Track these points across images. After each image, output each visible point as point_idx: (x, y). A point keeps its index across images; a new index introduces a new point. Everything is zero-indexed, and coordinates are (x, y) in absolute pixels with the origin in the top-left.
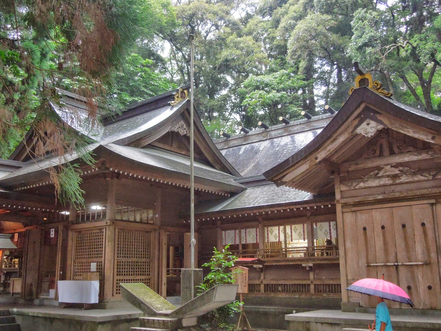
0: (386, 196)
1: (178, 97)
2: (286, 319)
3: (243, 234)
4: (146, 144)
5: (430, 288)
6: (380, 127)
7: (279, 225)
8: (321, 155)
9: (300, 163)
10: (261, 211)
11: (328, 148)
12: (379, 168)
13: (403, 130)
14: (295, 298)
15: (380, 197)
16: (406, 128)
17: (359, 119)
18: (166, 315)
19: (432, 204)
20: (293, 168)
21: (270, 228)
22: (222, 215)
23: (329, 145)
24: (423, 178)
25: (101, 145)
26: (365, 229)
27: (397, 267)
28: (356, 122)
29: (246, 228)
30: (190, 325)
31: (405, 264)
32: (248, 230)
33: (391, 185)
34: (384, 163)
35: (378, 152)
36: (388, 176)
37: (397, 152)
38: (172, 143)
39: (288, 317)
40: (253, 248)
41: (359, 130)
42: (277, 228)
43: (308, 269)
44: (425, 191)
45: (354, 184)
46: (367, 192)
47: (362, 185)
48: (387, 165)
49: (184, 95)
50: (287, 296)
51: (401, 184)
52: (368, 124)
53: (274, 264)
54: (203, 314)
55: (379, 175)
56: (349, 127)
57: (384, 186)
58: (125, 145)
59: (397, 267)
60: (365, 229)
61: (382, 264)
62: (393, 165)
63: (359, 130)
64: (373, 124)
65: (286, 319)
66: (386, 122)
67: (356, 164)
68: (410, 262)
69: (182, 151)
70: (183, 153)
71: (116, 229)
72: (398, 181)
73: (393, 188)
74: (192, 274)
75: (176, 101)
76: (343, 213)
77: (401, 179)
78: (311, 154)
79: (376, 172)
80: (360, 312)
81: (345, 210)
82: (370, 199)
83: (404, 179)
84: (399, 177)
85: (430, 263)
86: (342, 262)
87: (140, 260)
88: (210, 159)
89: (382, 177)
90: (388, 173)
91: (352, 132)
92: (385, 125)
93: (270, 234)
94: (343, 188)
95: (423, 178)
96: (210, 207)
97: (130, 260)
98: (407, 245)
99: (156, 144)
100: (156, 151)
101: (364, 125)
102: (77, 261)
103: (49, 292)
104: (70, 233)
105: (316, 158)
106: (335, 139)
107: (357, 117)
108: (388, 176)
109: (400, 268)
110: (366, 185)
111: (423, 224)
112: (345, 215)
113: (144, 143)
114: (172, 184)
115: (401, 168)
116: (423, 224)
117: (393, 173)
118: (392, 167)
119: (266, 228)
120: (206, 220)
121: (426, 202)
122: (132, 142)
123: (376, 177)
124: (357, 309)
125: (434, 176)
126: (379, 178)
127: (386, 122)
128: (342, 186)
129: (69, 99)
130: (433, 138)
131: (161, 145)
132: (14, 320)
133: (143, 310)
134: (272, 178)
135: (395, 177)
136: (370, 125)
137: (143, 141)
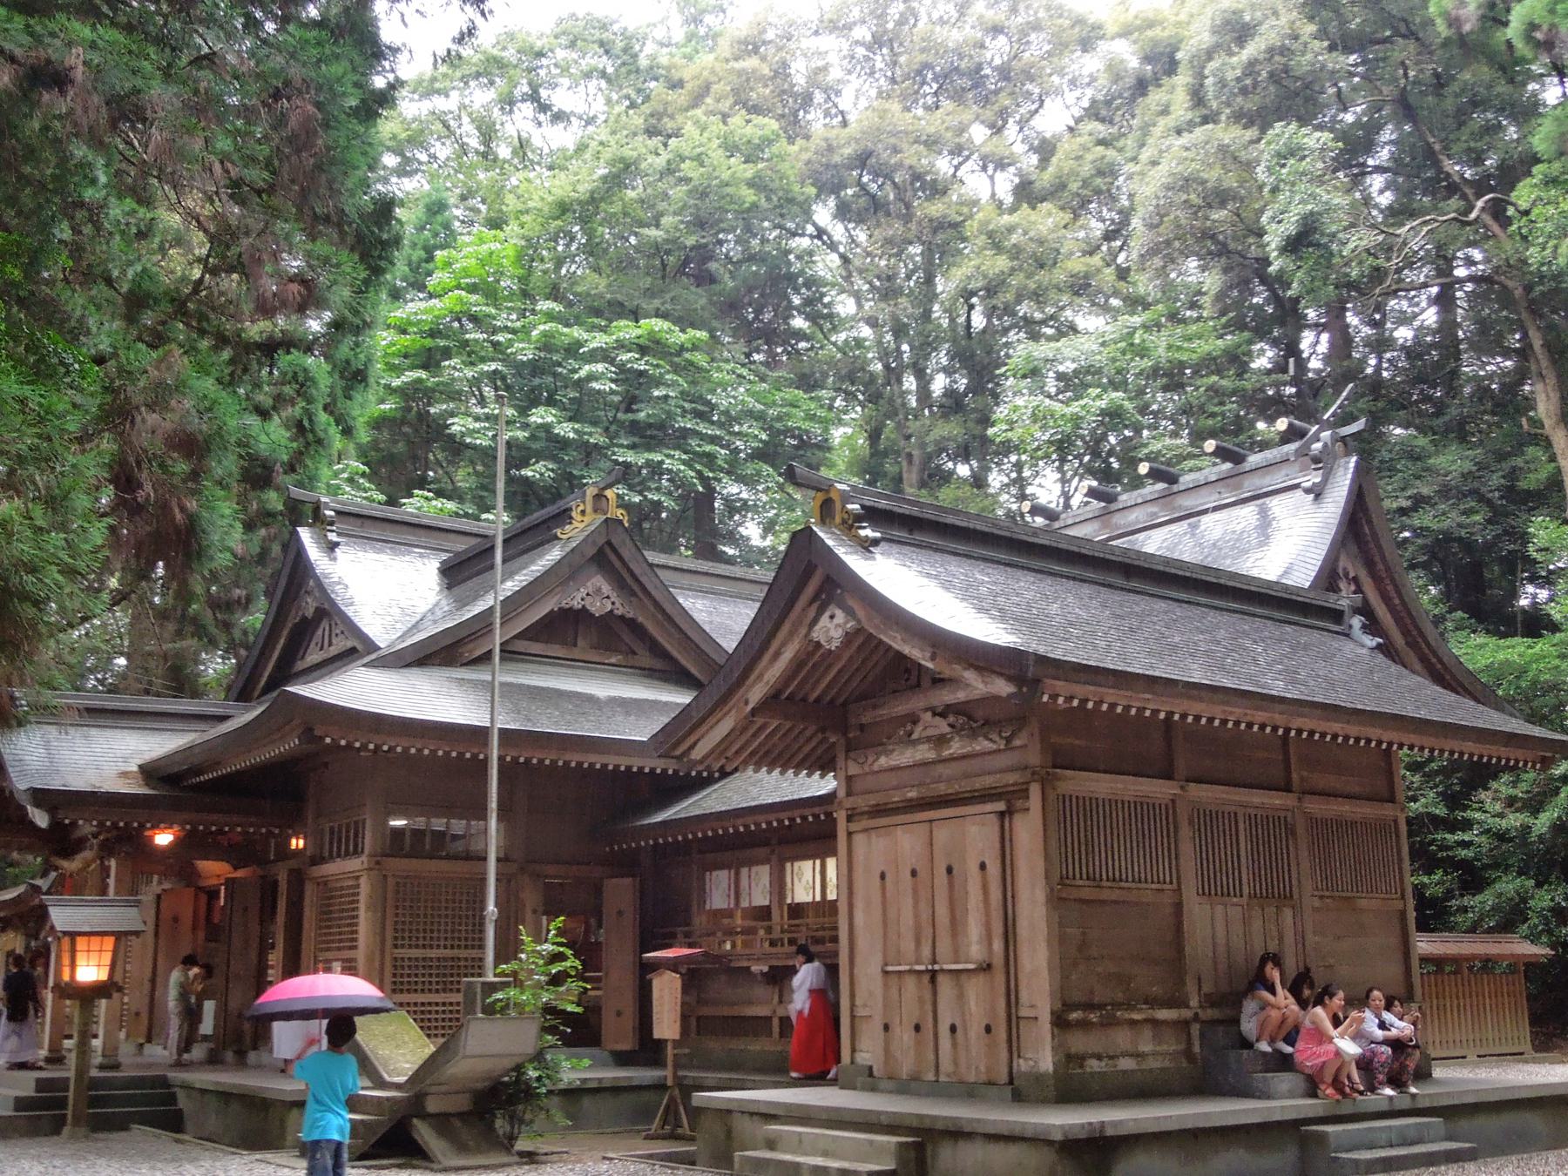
0: (925, 792)
3: (744, 882)
4: (478, 653)
7: (812, 857)
10: (797, 814)
11: (766, 677)
15: (912, 794)
17: (816, 605)
18: (398, 1086)
19: (1002, 814)
20: (704, 728)
21: (796, 864)
22: (726, 824)
23: (767, 668)
26: (883, 876)
27: (933, 975)
28: (812, 613)
29: (751, 863)
30: (451, 1110)
31: (946, 967)
32: (754, 869)
33: (933, 763)
34: (922, 704)
36: (929, 739)
38: (576, 639)
39: (701, 1097)
40: (817, 916)
41: (817, 634)
44: (988, 781)
45: (870, 759)
46: (893, 780)
47: (883, 761)
48: (927, 710)
52: (832, 617)
55: (915, 736)
57: (925, 764)
58: (408, 666)
59: (933, 975)
60: (883, 876)
62: (939, 710)
63: (817, 634)
64: (840, 616)
65: (695, 1103)
66: (861, 613)
67: (875, 707)
68: (956, 962)
70: (613, 660)
72: (946, 753)
74: (479, 990)
75: (575, 524)
76: (850, 834)
80: (864, 1088)
81: (853, 827)
83: (956, 747)
85: (989, 966)
90: (930, 732)
92: (859, 621)
96: (649, 814)
97: (433, 953)
99: (521, 646)
100: (520, 665)
101: (824, 620)
103: (659, 1041)
105: (747, 703)
106: (777, 655)
107: (811, 603)
108: (929, 739)
109: (940, 978)
110: (893, 763)
113: (470, 652)
114: (528, 761)
115: (951, 719)
116: (983, 866)
117: (936, 732)
118: (935, 714)
119: (788, 865)
120: (705, 837)
121: (989, 807)
123: (908, 739)
124: (860, 1080)
125: (1008, 740)
126: (915, 743)
127: (861, 613)
129: (359, 522)
130: (933, 659)
131: (536, 648)
132: (172, 1099)
136: (836, 621)
137: (471, 646)
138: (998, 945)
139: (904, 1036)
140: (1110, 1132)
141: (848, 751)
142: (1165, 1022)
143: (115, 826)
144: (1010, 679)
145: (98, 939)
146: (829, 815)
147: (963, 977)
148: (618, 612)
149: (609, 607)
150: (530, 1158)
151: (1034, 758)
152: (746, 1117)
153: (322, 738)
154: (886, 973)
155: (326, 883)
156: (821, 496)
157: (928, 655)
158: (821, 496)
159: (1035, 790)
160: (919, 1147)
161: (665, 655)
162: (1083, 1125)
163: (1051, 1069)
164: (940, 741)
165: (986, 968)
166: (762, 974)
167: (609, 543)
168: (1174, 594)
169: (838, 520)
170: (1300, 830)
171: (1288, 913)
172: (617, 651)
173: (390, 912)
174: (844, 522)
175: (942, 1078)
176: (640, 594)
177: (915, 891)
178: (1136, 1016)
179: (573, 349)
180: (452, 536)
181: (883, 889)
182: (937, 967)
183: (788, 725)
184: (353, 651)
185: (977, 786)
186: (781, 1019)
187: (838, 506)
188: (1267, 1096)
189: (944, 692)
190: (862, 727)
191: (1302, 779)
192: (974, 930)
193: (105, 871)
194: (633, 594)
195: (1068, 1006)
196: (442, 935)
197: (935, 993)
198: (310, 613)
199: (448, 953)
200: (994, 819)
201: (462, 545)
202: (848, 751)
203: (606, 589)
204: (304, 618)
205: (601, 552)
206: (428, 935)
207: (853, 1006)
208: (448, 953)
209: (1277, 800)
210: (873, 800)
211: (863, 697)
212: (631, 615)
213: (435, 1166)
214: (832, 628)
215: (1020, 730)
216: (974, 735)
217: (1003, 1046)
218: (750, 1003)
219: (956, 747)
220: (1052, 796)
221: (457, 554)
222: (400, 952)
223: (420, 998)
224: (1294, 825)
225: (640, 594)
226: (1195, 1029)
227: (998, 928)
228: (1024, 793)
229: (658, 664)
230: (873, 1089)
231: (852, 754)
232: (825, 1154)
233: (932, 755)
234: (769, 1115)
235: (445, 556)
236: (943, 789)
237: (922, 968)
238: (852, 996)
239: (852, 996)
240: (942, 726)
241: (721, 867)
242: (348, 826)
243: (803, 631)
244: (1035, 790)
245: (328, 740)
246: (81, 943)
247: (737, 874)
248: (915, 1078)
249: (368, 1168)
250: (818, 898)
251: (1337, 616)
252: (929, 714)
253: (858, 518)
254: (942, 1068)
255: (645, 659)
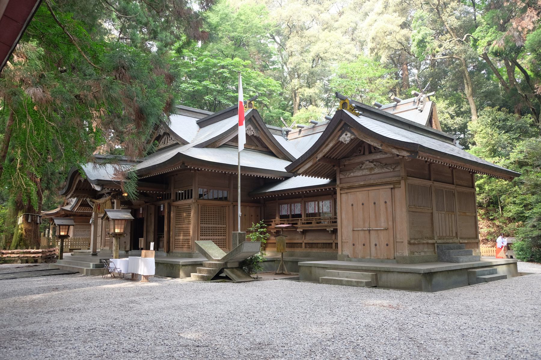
1: (246, 107)
2: (299, 264)
3: (293, 208)
5: (387, 245)
6: (353, 137)
7: (315, 201)
8: (320, 156)
9: (307, 161)
11: (323, 151)
12: (363, 163)
13: (366, 140)
14: (323, 253)
15: (362, 183)
16: (367, 138)
18: (218, 260)
19: (392, 188)
21: (283, 206)
23: (324, 149)
24: (388, 170)
25: (179, 153)
26: (352, 205)
29: (294, 203)
30: (234, 267)
31: (374, 229)
32: (296, 204)
34: (365, 159)
35: (362, 153)
36: (367, 169)
37: (373, 152)
39: (300, 263)
42: (314, 203)
43: (330, 232)
44: (388, 180)
45: (348, 174)
47: (352, 174)
48: (367, 161)
49: (251, 105)
50: (319, 251)
51: (375, 174)
52: (346, 135)
53: (310, 229)
54: (244, 260)
55: (362, 168)
56: (335, 136)
58: (203, 148)
60: (352, 205)
61: (361, 229)
62: (371, 161)
63: (341, 139)
64: (349, 134)
65: (299, 264)
66: (356, 133)
67: (349, 160)
69: (252, 147)
70: (252, 148)
71: (199, 206)
72: (373, 172)
73: (370, 176)
76: (341, 194)
77: (374, 171)
78: (313, 155)
79: (361, 165)
80: (347, 260)
81: (342, 192)
82: (172, 213)
84: (374, 169)
86: (339, 228)
87: (217, 226)
88: (274, 151)
89: (364, 169)
90: (367, 167)
91: (337, 140)
92: (355, 136)
93: (309, 207)
94: (342, 177)
95: (388, 170)
97: (210, 226)
98: (376, 216)
99: (230, 143)
101: (344, 135)
102: (177, 226)
104: (172, 208)
105: (317, 158)
107: (339, 130)
108: (367, 169)
109: (371, 232)
111: (386, 202)
112: (342, 195)
115: (375, 163)
116: (386, 202)
117: (370, 167)
118: (369, 162)
121: (388, 187)
122: (209, 145)
125: (394, 169)
127: (356, 133)
128: (341, 175)
130: (381, 146)
133: (207, 258)
134: (292, 170)
135: (371, 169)
136: (347, 136)
137: (218, 143)
138: (390, 223)
139: (359, 247)
140: (432, 271)
141: (340, 171)
142: (430, 243)
143: (115, 190)
144: (408, 151)
145: (120, 221)
146: (334, 189)
147: (379, 231)
148: (255, 135)
149: (253, 133)
150: (257, 279)
151: (403, 174)
152: (317, 268)
153: (187, 166)
154: (354, 230)
155: (178, 207)
156: (342, 102)
157: (379, 145)
158: (342, 102)
159: (403, 182)
160: (376, 275)
161: (268, 148)
162: (427, 269)
163: (407, 255)
164: (371, 169)
165: (386, 229)
166: (301, 232)
167: (253, 116)
168: (419, 133)
169: (348, 108)
170: (456, 195)
171: (453, 215)
172: (253, 145)
173: (200, 214)
174: (350, 109)
175: (372, 258)
176: (260, 130)
177: (386, 208)
178: (425, 242)
179: (215, 65)
180: (199, 114)
181: (353, 209)
182: (371, 229)
183: (325, 164)
184: (177, 144)
185: (384, 181)
186: (336, 243)
187: (348, 104)
188: (458, 262)
189: (373, 156)
190: (345, 165)
191: (456, 182)
192: (383, 219)
193: (113, 203)
194: (259, 130)
195: (411, 239)
196: (213, 221)
197: (370, 236)
198: (162, 134)
199: (214, 226)
200: (390, 190)
201: (202, 117)
202: (340, 171)
203: (252, 129)
204: (160, 135)
205: (250, 118)
206: (216, 221)
207: (342, 239)
208: (214, 226)
209: (451, 187)
210: (349, 185)
211: (344, 158)
212: (258, 136)
213: (233, 281)
214: (346, 138)
215: (398, 166)
216: (382, 167)
217: (392, 250)
218: (295, 239)
219: (376, 171)
220: (406, 184)
221: (201, 119)
222: (202, 225)
223: (218, 237)
224: (454, 193)
225: (260, 130)
226: (436, 245)
227: (390, 219)
228: (399, 183)
229: (264, 149)
230: (350, 261)
231: (341, 173)
232: (347, 277)
233: (368, 173)
234: (325, 267)
235: (197, 120)
236: (372, 182)
237: (366, 229)
238: (342, 236)
239: (342, 236)
240: (372, 165)
241: (312, 201)
242: (188, 190)
243: (336, 138)
244: (403, 182)
245: (189, 167)
246: (61, 227)
247: (291, 206)
248: (363, 258)
249: (217, 282)
250: (317, 211)
251: (452, 140)
252: (368, 162)
253: (355, 108)
254: (372, 255)
255: (260, 148)
